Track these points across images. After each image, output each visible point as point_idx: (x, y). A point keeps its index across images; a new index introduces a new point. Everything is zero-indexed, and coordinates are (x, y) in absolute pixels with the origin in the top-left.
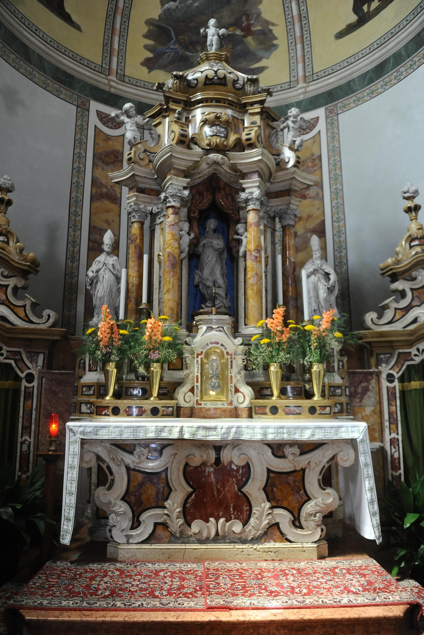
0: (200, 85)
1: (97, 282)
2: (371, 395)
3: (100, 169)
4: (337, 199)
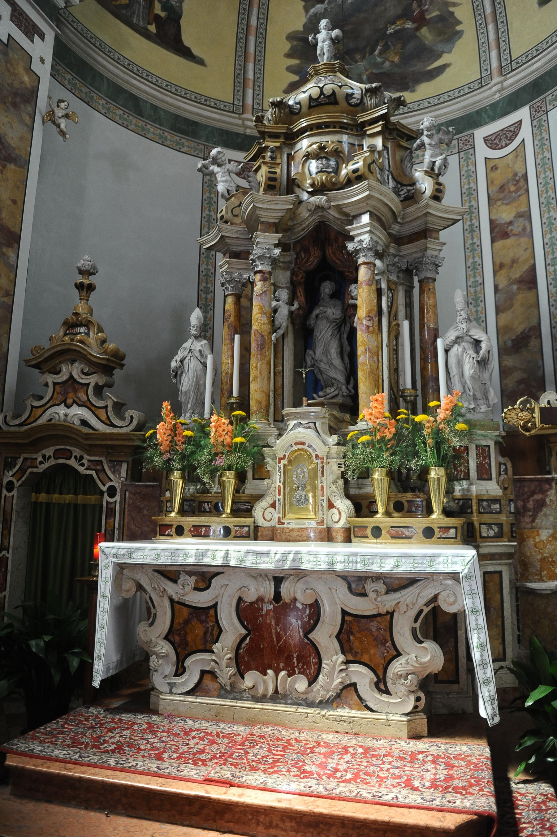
0: (305, 109)
1: (182, 373)
2: (548, 513)
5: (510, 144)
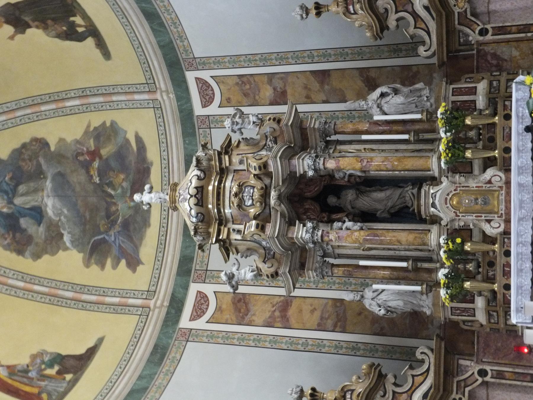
0: (202, 210)
1: (389, 307)
2: (500, 51)
3: (254, 318)
4: (288, 58)
5: (212, 88)
